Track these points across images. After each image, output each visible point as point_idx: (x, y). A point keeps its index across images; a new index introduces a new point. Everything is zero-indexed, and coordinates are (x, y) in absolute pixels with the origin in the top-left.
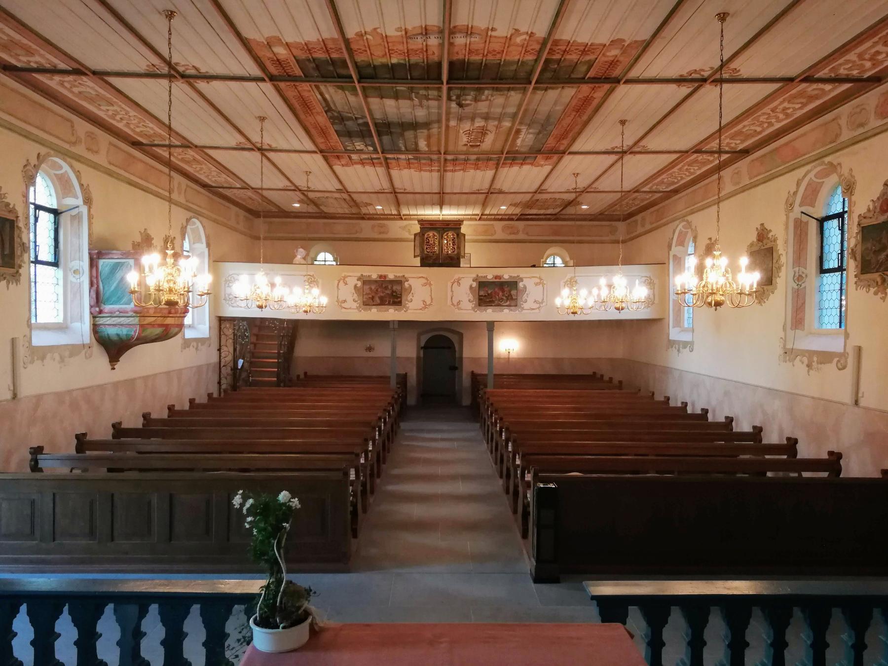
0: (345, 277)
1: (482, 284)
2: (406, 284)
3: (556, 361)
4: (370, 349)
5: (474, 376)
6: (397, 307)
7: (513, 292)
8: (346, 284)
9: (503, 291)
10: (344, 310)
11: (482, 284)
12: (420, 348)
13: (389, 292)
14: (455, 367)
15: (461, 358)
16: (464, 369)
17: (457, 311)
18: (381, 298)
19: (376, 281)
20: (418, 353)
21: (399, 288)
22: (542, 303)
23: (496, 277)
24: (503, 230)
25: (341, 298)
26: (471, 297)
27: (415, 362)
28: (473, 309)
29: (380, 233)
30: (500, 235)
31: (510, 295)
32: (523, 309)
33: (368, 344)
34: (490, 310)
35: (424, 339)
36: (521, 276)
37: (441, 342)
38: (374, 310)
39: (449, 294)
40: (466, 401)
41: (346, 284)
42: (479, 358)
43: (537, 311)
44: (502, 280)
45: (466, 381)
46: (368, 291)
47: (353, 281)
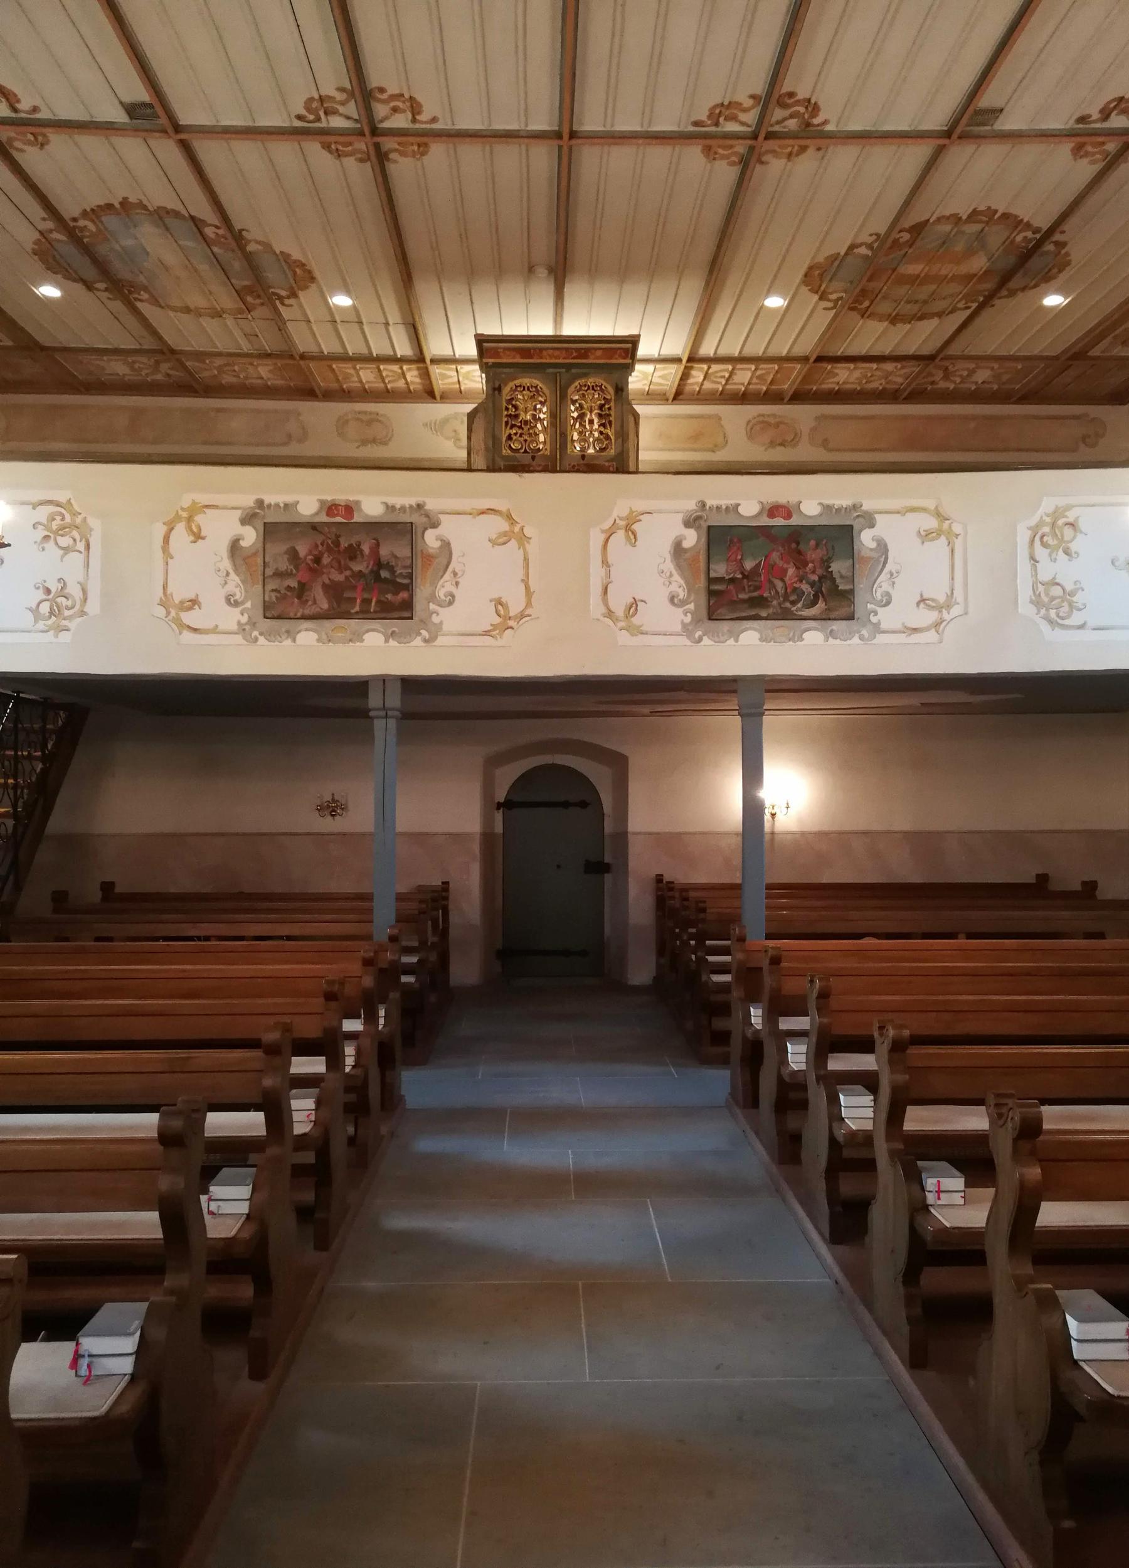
0: (194, 510)
1: (721, 537)
2: (431, 539)
3: (922, 842)
4: (333, 808)
5: (668, 896)
6: (396, 625)
7: (838, 567)
8: (198, 536)
9: (801, 562)
10: (187, 636)
11: (721, 537)
12: (492, 806)
13: (356, 569)
14: (601, 863)
15: (622, 837)
16: (633, 863)
17: (624, 638)
18: (334, 591)
19: (314, 527)
20: (487, 821)
21: (403, 552)
22: (948, 607)
23: (774, 510)
24: (751, 436)
25: (179, 592)
26: (678, 586)
27: (476, 848)
28: (687, 630)
29: (364, 442)
30: (740, 449)
31: (828, 576)
32: (877, 629)
33: (326, 790)
34: (750, 635)
35: (507, 776)
36: (867, 506)
37: (558, 749)
38: (307, 636)
39: (596, 573)
40: (641, 970)
41: (198, 536)
42: (679, 835)
43: (932, 636)
44: (795, 521)
45: (639, 907)
46: (284, 565)
47: (225, 527)
